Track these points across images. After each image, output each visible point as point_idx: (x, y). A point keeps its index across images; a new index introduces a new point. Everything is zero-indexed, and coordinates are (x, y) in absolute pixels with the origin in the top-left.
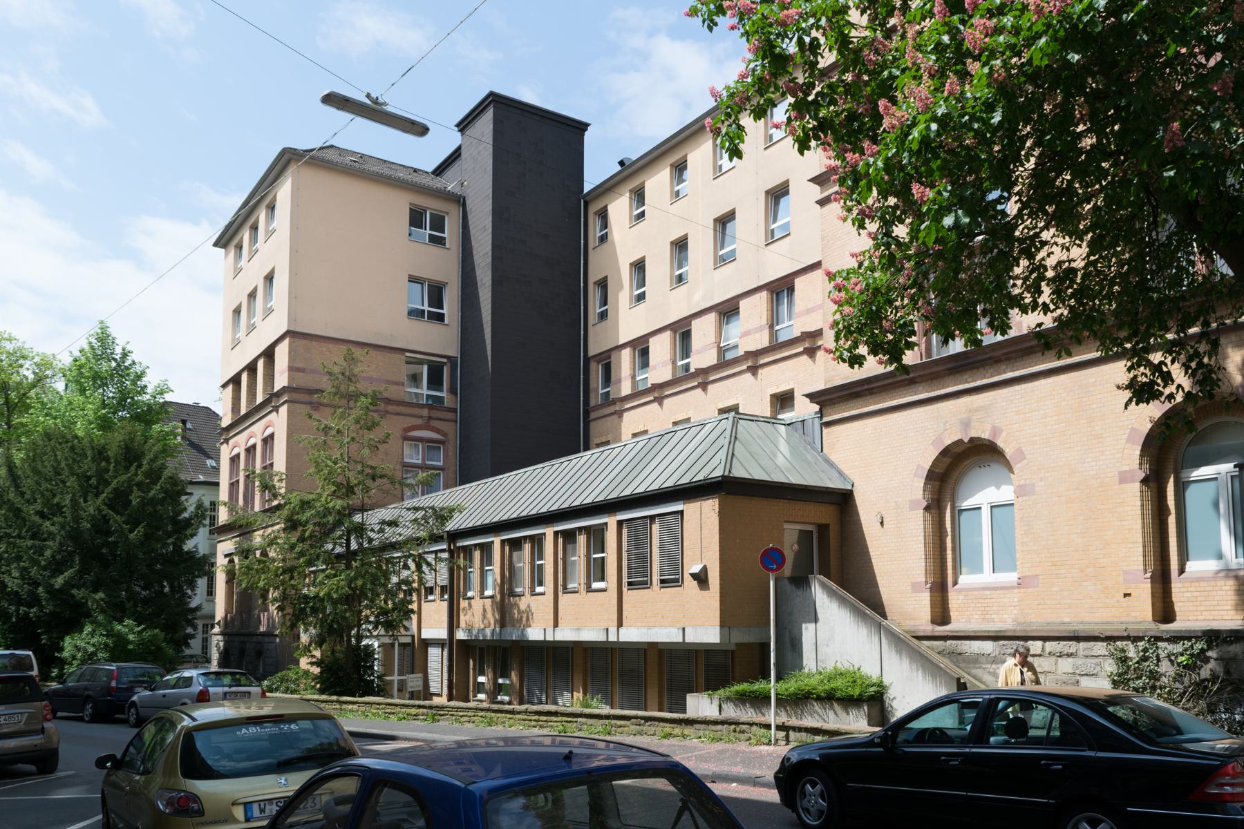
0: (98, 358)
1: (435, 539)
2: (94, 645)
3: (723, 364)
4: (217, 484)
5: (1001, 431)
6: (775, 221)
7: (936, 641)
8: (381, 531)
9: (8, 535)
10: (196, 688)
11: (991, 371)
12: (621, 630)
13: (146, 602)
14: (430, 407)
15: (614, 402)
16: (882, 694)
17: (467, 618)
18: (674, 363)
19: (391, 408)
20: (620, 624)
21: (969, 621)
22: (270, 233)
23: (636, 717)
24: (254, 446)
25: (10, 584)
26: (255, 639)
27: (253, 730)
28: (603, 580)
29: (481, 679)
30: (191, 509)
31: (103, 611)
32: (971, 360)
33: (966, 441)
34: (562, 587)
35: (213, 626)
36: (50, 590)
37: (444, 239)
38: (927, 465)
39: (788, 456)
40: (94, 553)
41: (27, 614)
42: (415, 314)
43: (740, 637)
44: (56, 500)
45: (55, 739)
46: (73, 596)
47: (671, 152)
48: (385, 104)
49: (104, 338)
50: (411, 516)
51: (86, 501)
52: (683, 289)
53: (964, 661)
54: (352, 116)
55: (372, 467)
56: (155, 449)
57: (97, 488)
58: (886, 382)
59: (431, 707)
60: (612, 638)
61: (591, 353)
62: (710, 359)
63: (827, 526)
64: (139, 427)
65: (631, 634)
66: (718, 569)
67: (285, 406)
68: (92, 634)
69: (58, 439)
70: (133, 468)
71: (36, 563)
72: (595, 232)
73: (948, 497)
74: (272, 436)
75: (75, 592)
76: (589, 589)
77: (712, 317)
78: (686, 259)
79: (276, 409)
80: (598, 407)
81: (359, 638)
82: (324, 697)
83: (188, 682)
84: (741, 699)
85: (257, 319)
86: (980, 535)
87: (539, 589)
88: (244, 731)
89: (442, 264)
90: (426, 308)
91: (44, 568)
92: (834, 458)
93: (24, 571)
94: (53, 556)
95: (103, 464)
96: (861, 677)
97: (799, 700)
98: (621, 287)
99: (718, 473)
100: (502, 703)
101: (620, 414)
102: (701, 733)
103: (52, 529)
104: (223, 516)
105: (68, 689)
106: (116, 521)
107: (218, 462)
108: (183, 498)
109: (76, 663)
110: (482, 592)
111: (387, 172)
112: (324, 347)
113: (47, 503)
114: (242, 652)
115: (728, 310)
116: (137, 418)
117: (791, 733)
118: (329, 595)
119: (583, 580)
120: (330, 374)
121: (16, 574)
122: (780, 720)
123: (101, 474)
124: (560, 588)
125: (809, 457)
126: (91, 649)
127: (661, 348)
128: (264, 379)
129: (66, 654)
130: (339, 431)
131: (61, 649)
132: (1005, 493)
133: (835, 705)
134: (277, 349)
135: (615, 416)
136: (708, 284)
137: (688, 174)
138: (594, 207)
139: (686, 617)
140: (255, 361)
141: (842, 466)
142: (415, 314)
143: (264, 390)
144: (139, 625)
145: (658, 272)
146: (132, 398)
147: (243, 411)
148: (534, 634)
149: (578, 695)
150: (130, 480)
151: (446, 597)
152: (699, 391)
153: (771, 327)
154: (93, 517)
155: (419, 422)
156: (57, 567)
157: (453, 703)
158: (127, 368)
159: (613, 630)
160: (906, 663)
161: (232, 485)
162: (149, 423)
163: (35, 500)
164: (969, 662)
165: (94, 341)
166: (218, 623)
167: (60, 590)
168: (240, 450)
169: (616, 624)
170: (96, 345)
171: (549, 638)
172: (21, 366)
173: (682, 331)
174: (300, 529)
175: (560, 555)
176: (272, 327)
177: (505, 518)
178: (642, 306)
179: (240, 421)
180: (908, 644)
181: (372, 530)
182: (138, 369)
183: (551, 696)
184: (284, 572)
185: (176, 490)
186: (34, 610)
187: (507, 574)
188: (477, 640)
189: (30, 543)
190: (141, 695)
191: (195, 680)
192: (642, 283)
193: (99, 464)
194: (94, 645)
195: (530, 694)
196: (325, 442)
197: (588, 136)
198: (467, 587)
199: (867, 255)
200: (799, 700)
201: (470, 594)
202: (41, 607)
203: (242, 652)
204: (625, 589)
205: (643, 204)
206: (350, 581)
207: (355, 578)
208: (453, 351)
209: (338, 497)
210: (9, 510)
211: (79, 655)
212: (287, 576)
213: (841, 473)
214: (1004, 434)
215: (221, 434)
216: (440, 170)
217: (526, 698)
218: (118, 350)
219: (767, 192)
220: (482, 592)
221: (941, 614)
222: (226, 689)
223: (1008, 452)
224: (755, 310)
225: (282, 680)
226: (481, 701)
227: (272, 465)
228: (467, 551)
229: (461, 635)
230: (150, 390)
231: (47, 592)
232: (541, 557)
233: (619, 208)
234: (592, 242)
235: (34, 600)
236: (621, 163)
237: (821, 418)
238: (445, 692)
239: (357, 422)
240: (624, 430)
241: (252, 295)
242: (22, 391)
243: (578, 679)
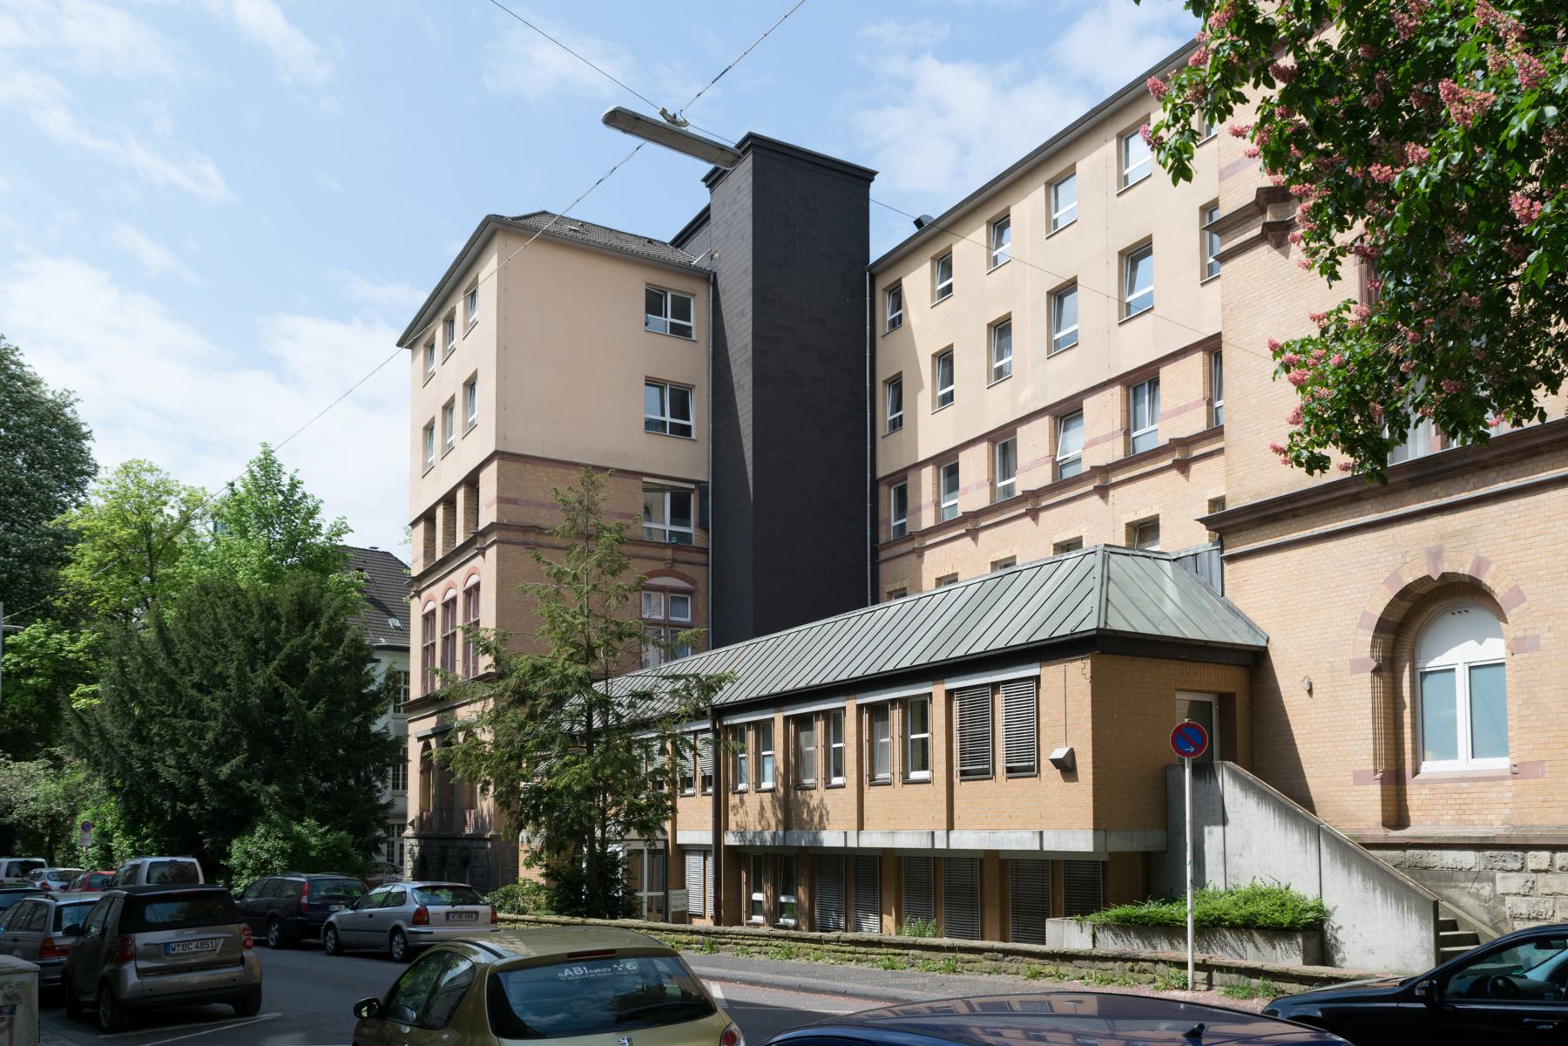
0: (262, 491)
1: (699, 715)
2: (268, 851)
3: (1059, 484)
4: (407, 650)
5: (1489, 563)
6: (1131, 292)
7: (1393, 854)
8: (632, 705)
9: (162, 714)
10: (412, 907)
11: (1473, 481)
12: (952, 834)
13: (326, 796)
14: (675, 547)
15: (912, 537)
16: (1322, 922)
17: (739, 818)
18: (992, 484)
20: (950, 826)
21: (1437, 823)
22: (470, 327)
23: (991, 950)
24: (454, 600)
25: (164, 774)
26: (459, 843)
27: (578, 971)
28: (925, 767)
29: (757, 896)
30: (380, 680)
31: (278, 808)
32: (1444, 467)
33: (1436, 577)
34: (868, 777)
35: (403, 827)
36: (214, 783)
37: (690, 328)
38: (1378, 611)
39: (1178, 601)
40: (265, 735)
41: (185, 811)
42: (652, 426)
43: (1119, 844)
44: (218, 669)
45: (256, 972)
46: (241, 789)
47: (988, 205)
48: (685, 123)
49: (268, 465)
50: (667, 686)
51: (253, 671)
52: (1005, 386)
53: (1432, 878)
54: (639, 141)
55: (618, 624)
56: (335, 604)
57: (266, 653)
58: (1318, 499)
59: (692, 932)
60: (940, 844)
61: (881, 473)
62: (1043, 477)
63: (1231, 696)
64: (314, 577)
65: (966, 839)
66: (1090, 754)
67: (494, 548)
68: (266, 837)
69: (218, 592)
70: (308, 629)
71: (196, 747)
72: (885, 314)
73: (1406, 655)
74: (477, 586)
75: (243, 784)
76: (906, 781)
77: (1045, 422)
78: (1010, 347)
79: (482, 551)
80: (890, 544)
81: (605, 842)
82: (564, 919)
83: (400, 899)
84: (1124, 926)
85: (455, 438)
86: (1457, 706)
87: (836, 781)
88: (567, 972)
89: (687, 362)
90: (668, 418)
91: (206, 755)
92: (1239, 604)
93: (181, 758)
94: (216, 740)
95: (274, 623)
96: (1291, 899)
97: (1209, 927)
98: (920, 386)
99: (1090, 625)
100: (785, 927)
101: (920, 552)
102: (1084, 972)
103: (215, 705)
104: (416, 692)
105: (248, 905)
106: (291, 695)
108: (369, 666)
109: (245, 872)
110: (758, 784)
111: (616, 243)
113: (207, 673)
114: (444, 860)
115: (1066, 413)
116: (309, 565)
117: (1215, 974)
118: (567, 787)
119: (898, 769)
120: (565, 503)
121: (171, 761)
122: (1200, 957)
123: (270, 635)
124: (866, 779)
125: (1205, 603)
126: (265, 856)
127: (975, 466)
129: (233, 861)
130: (575, 577)
131: (228, 856)
132: (1492, 649)
133: (1256, 935)
134: (482, 476)
135: (914, 556)
136: (1039, 378)
137: (1010, 233)
138: (883, 283)
139: (1054, 818)
140: (453, 492)
141: (1250, 615)
142: (652, 426)
143: (466, 528)
144: (321, 826)
145: (971, 364)
146: (304, 541)
147: (439, 556)
148: (831, 838)
149: (889, 921)
150: (305, 644)
151: (710, 790)
152: (1028, 520)
153: (1127, 433)
154: (263, 690)
155: (661, 566)
156: (221, 753)
157: (721, 928)
158: (297, 503)
159: (940, 835)
160: (1357, 880)
161: (426, 649)
162: (325, 572)
163: (192, 670)
164: (1439, 880)
165: (256, 469)
166: (412, 824)
167: (225, 782)
168: (437, 604)
169: (855, 824)
170: (258, 473)
171: (852, 844)
172: (165, 504)
173: (1002, 442)
174: (530, 702)
175: (866, 736)
176: (480, 444)
177: (753, 695)
178: (950, 410)
179: (434, 569)
180: (1356, 853)
181: (620, 704)
182: (310, 503)
183: (852, 917)
184: (511, 758)
185: (362, 656)
186: (194, 806)
187: (792, 760)
188: (753, 847)
189: (188, 723)
190: (341, 914)
191: (409, 897)
192: (949, 379)
193: (268, 623)
194: (268, 851)
195: (824, 917)
196: (558, 592)
197: (875, 189)
198: (738, 778)
199: (1333, 318)
200: (1209, 927)
201: (741, 787)
202: (202, 803)
203: (444, 860)
204: (956, 780)
205: (950, 276)
206: (596, 769)
207: (603, 765)
208: (703, 473)
209: (577, 662)
210: (160, 683)
211: (250, 863)
212: (513, 764)
213: (1250, 625)
214: (1493, 568)
215: (410, 585)
216: (681, 240)
217: (818, 922)
218: (286, 480)
219: (1121, 253)
220: (758, 784)
221: (1396, 815)
222: (449, 908)
223: (1500, 591)
224: (1104, 412)
225: (507, 896)
226: (757, 925)
227: (477, 623)
228: (739, 731)
229: (730, 840)
230: (324, 531)
231: (210, 784)
232: (838, 739)
233: (917, 281)
234: (881, 328)
235: (195, 794)
236: (919, 223)
237: (1222, 550)
238: (710, 911)
239: (599, 565)
240: (925, 574)
241: (448, 407)
242: (167, 535)
243: (889, 898)
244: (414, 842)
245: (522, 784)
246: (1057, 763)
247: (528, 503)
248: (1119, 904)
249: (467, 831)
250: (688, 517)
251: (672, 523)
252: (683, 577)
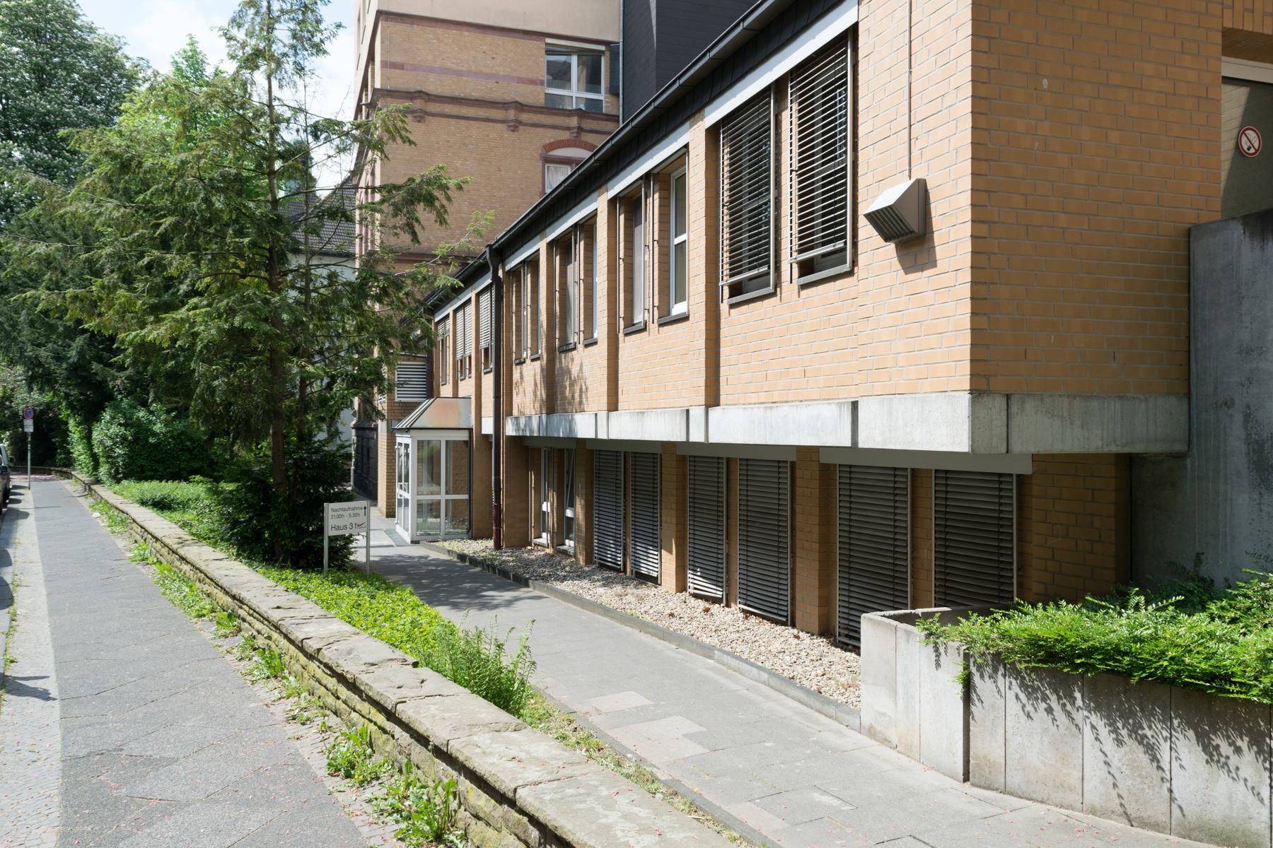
19: (525, 117)
43: (1046, 431)
112: (431, 33)
126: (109, 443)
148: (584, 427)
155: (565, 135)
159: (697, 413)
208: (614, 34)
246: (886, 222)
247: (415, 68)
248: (1049, 597)
249: (398, 490)
250: (599, 83)
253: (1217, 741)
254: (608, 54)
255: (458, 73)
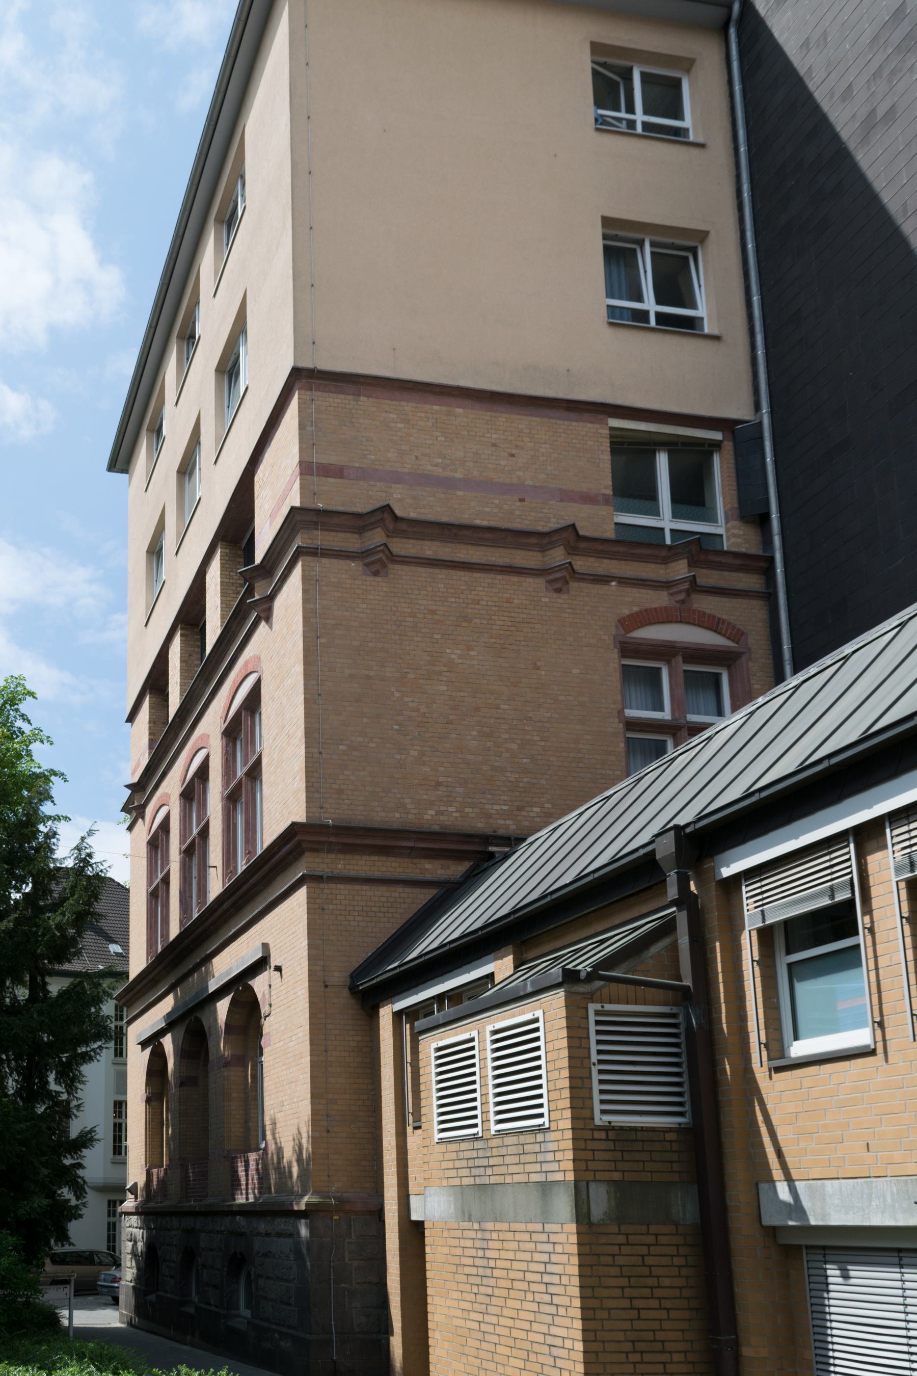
107: (126, 945)
128: (223, 593)
155: (660, 600)
244: (134, 1220)
245: (19, 1300)
247: (365, 474)
249: (241, 1199)
251: (676, 515)
252: (713, 624)
253: (74, 1133)
254: (728, 446)
255: (448, 484)
